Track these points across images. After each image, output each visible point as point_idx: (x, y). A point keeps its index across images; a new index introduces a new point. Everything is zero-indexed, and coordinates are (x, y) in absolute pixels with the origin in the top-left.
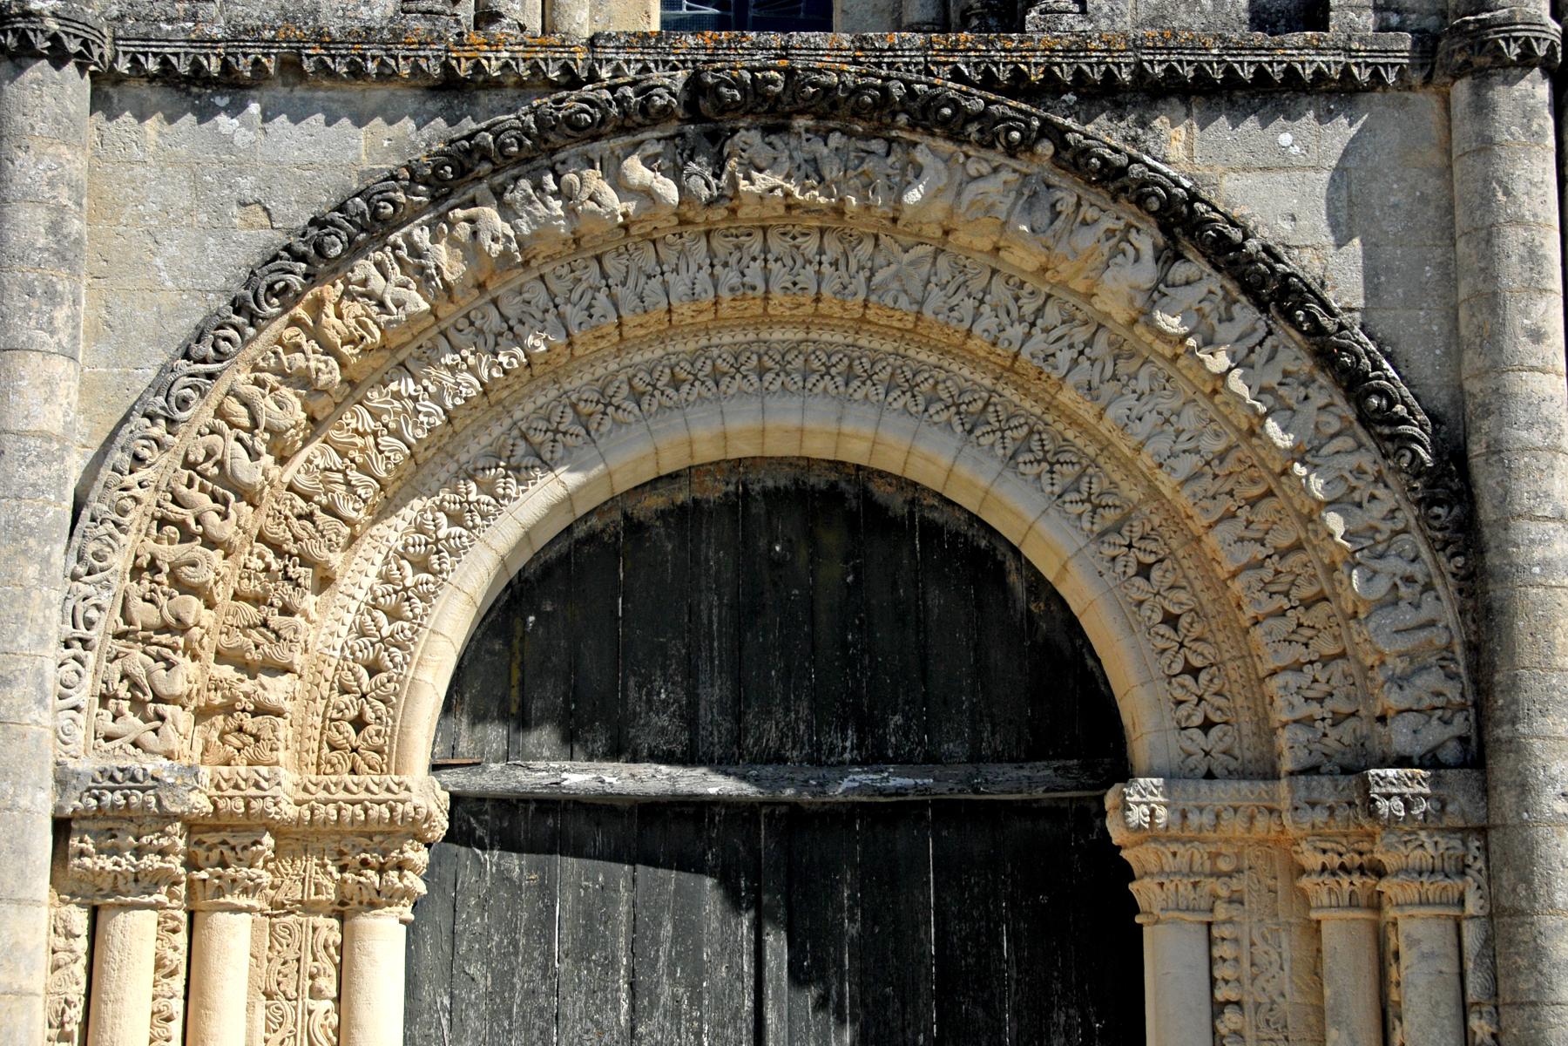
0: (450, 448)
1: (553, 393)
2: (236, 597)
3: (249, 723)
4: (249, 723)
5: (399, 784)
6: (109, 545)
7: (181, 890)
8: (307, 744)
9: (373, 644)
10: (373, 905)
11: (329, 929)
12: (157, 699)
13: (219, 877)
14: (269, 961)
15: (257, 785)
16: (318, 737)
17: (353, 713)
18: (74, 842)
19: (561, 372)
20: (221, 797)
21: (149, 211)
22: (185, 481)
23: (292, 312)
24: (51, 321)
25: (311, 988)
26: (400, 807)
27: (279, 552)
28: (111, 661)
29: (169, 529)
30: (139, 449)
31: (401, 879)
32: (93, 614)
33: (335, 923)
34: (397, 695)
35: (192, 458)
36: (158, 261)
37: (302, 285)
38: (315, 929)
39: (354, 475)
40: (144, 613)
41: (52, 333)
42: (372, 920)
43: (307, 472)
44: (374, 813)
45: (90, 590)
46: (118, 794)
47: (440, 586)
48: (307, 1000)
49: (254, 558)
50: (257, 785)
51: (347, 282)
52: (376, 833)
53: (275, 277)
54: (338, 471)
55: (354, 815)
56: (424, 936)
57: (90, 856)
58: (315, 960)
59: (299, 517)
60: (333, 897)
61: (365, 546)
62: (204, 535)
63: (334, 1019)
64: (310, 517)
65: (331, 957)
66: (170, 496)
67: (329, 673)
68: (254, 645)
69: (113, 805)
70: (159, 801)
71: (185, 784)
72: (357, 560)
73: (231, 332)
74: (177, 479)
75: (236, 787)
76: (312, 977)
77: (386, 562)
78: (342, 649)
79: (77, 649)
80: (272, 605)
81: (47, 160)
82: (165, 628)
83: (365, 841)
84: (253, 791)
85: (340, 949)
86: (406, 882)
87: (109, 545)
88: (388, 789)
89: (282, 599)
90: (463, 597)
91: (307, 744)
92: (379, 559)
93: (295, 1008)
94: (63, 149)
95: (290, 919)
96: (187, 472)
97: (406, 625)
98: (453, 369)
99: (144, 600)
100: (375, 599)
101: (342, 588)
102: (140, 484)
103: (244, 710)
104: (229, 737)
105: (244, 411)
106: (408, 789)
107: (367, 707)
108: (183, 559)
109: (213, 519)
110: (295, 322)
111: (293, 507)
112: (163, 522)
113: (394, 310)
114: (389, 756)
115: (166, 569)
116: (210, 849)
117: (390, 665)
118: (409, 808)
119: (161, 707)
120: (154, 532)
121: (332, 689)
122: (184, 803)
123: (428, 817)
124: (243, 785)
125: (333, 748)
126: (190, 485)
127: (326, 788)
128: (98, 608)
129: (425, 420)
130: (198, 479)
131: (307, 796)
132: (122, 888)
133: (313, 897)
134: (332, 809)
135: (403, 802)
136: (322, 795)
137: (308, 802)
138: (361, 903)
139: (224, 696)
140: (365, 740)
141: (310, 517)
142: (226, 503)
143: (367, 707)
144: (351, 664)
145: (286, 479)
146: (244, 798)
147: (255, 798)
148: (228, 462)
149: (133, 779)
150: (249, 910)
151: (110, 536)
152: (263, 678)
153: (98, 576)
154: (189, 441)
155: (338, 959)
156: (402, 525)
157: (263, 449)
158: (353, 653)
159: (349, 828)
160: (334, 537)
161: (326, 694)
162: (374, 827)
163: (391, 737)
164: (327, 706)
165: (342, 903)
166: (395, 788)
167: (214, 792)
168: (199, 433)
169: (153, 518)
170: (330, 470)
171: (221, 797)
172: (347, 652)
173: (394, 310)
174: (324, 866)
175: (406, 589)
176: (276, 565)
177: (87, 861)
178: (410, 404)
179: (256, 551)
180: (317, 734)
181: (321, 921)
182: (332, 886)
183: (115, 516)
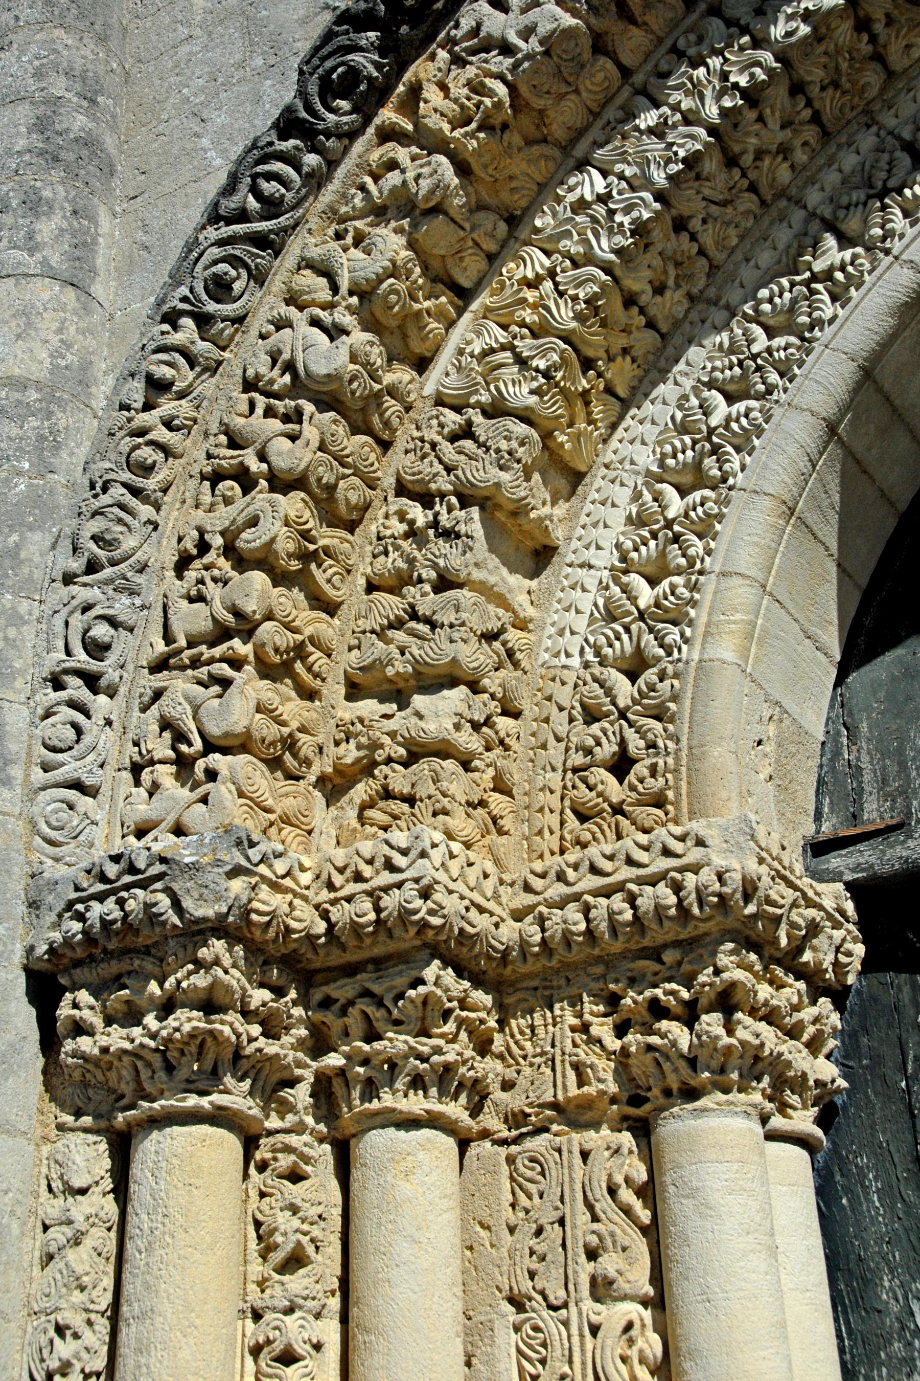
0: (712, 292)
1: (867, 141)
2: (371, 588)
3: (399, 779)
4: (399, 779)
5: (682, 839)
6: (120, 521)
7: (301, 1095)
8: (541, 820)
9: (628, 630)
10: (691, 1094)
11: (612, 1152)
12: (210, 747)
13: (365, 1062)
14: (512, 1230)
15: (390, 867)
16: (557, 806)
17: (608, 749)
18: (64, 1011)
19: (877, 106)
20: (334, 902)
22: (244, 407)
23: (377, 121)
24: (30, 236)
25: (593, 1280)
26: (690, 880)
27: (426, 500)
28: (144, 710)
30: (153, 368)
31: (730, 1032)
32: (101, 631)
33: (626, 1139)
34: (675, 698)
35: (250, 373)
36: (205, 142)
37: (378, 66)
38: (585, 1155)
39: (525, 346)
40: (190, 619)
41: (31, 252)
42: (702, 1123)
43: (459, 369)
44: (645, 903)
45: (93, 594)
46: (110, 902)
47: (727, 502)
48: (588, 1304)
49: (394, 521)
50: (390, 867)
51: (451, 42)
52: (665, 946)
53: (329, 64)
54: (503, 348)
55: (611, 914)
56: (862, 1176)
57: (91, 1033)
58: (595, 1219)
59: (453, 438)
60: (612, 1088)
61: (598, 482)
63: (652, 1344)
64: (467, 432)
65: (627, 1211)
66: (223, 439)
67: (564, 695)
68: (398, 656)
69: (106, 924)
70: (177, 904)
71: (218, 863)
72: (589, 507)
73: (277, 166)
74: (230, 410)
75: (358, 877)
76: (592, 1255)
77: (637, 496)
78: (582, 652)
79: (76, 688)
80: (420, 581)
81: (34, 49)
82: (222, 634)
83: (649, 966)
84: (387, 878)
85: (648, 1192)
86: (741, 1033)
87: (120, 521)
88: (667, 852)
89: (435, 566)
90: (767, 502)
91: (541, 820)
92: (623, 495)
93: (566, 1323)
94: (59, 33)
95: (538, 1144)
96: (245, 396)
97: (679, 580)
98: (658, 132)
99: (191, 600)
100: (624, 559)
101: (571, 558)
103: (389, 760)
104: (369, 813)
105: (323, 282)
106: (700, 843)
107: (630, 733)
108: (240, 520)
110: (387, 135)
111: (442, 426)
112: (215, 478)
113: (521, 44)
114: (676, 804)
115: (218, 541)
116: (344, 1012)
117: (661, 652)
118: (707, 876)
119: (216, 760)
120: (207, 499)
121: (571, 720)
122: (218, 900)
123: (749, 890)
124: (367, 871)
125: (583, 818)
127: (561, 877)
128: (113, 622)
129: (626, 220)
130: (261, 402)
131: (530, 899)
132: (148, 1087)
133: (573, 1091)
134: (573, 913)
135: (695, 869)
136: (557, 890)
137: (530, 909)
138: (667, 1093)
139: (359, 747)
140: (632, 788)
141: (467, 432)
143: (630, 733)
144: (597, 670)
145: (429, 389)
146: (370, 894)
147: (386, 889)
149: (132, 869)
150: (433, 1121)
151: (123, 507)
152: (418, 701)
153: (108, 572)
155: (645, 1216)
156: (650, 432)
158: (598, 654)
159: (618, 946)
160: (504, 445)
161: (562, 730)
162: (656, 936)
163: (676, 771)
164: (567, 749)
165: (636, 1100)
166: (678, 847)
167: (325, 895)
168: (263, 337)
169: (203, 477)
170: (493, 351)
171: (334, 902)
172: (590, 656)
173: (521, 44)
174: (585, 1028)
175: (669, 524)
176: (419, 515)
177: (85, 1043)
178: (600, 210)
179: (393, 508)
180: (554, 801)
181: (600, 1138)
182: (605, 1068)
183: (126, 476)
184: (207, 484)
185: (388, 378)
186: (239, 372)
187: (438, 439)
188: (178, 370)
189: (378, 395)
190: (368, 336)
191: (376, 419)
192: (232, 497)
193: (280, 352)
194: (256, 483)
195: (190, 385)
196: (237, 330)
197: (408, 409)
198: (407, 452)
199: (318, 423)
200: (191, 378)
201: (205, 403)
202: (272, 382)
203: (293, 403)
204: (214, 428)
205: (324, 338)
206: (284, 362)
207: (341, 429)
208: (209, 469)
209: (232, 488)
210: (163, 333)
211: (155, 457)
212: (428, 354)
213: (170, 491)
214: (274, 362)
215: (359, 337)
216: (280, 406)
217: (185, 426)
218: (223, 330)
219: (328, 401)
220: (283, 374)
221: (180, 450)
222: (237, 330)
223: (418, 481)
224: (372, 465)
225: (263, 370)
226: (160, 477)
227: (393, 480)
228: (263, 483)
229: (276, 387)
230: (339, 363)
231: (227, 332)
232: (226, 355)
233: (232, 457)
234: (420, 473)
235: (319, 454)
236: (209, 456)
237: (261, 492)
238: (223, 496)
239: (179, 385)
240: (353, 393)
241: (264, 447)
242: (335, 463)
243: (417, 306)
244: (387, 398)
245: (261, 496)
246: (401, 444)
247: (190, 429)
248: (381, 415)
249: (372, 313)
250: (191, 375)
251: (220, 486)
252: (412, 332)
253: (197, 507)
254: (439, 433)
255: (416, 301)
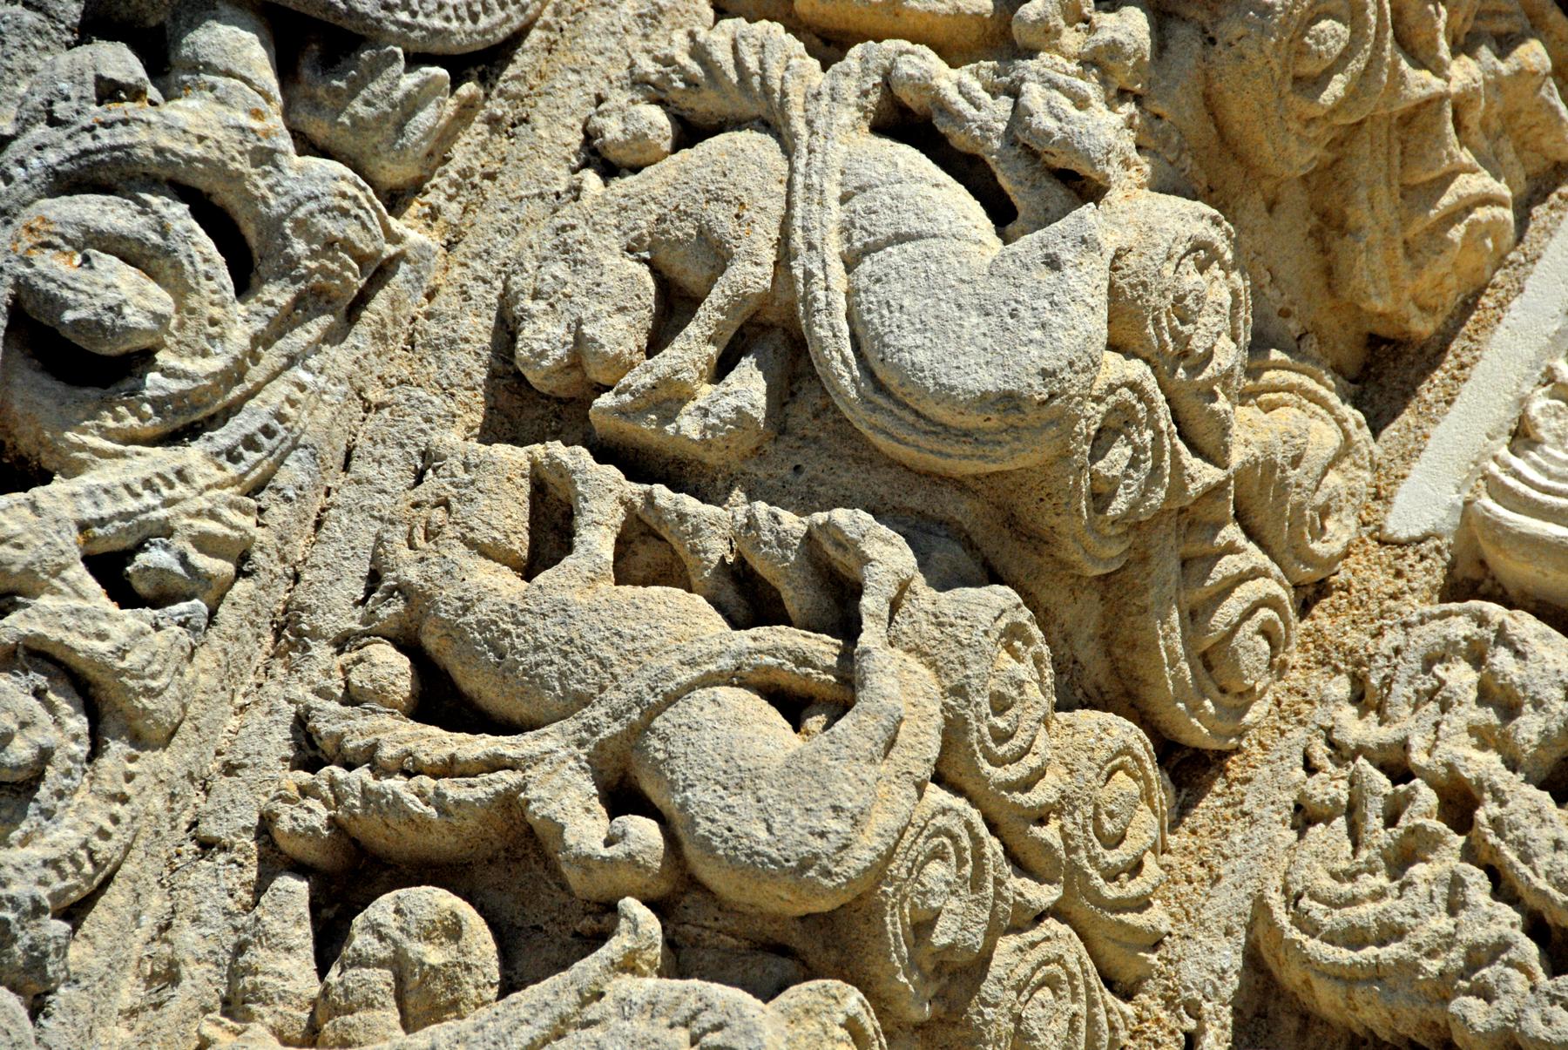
21: (990, 5)
22: (508, 517)
29: (407, 916)
30: (56, 266)
35: (543, 337)
62: (680, 894)
66: (390, 666)
96: (512, 457)
102: (111, 569)
109: (731, 745)
112: (347, 877)
120: (292, 970)
126: (552, 528)
130: (605, 496)
142: (838, 601)
145: (1425, 503)
148: (831, 287)
154: (511, 233)
157: (1104, 128)
168: (601, 159)
169: (275, 857)
184: (294, 891)
185: (1251, 432)
186: (478, 327)
187: (1484, 764)
188: (180, 289)
189: (1192, 519)
190: (1187, 218)
191: (1170, 634)
192: (449, 977)
193: (717, 255)
194: (604, 916)
195: (234, 374)
196: (467, 110)
197: (1310, 595)
198: (1305, 816)
199: (937, 641)
200: (239, 337)
201: (293, 473)
202: (667, 399)
203: (793, 523)
204: (337, 602)
205: (957, 205)
206: (739, 300)
207: (1028, 675)
208: (318, 815)
209: (453, 930)
210: (109, 91)
211: (46, 734)
212: (1423, 327)
213: (99, 913)
214: (674, 307)
215: (1146, 220)
216: (713, 526)
217: (197, 583)
218: (411, 105)
219: (974, 537)
220: (721, 369)
221: (165, 707)
222: (467, 110)
223: (1376, 973)
224: (1136, 868)
225: (618, 333)
226: (63, 835)
227: (1230, 956)
228: (641, 923)
229: (689, 425)
230: (1068, 344)
231: (426, 118)
232: (412, 230)
233: (450, 768)
234: (1391, 933)
235: (937, 796)
236: (310, 750)
237: (628, 965)
238: (399, 964)
239: (179, 369)
240: (1100, 499)
241: (640, 730)
242: (993, 845)
243: (1421, 84)
244: (1232, 532)
245: (626, 984)
246: (1268, 774)
247: (216, 591)
248: (1195, 617)
249: (1211, 105)
250: (243, 325)
251: (382, 909)
252: (1372, 210)
253: (235, 1006)
254: (1483, 738)
255: (1422, 58)
